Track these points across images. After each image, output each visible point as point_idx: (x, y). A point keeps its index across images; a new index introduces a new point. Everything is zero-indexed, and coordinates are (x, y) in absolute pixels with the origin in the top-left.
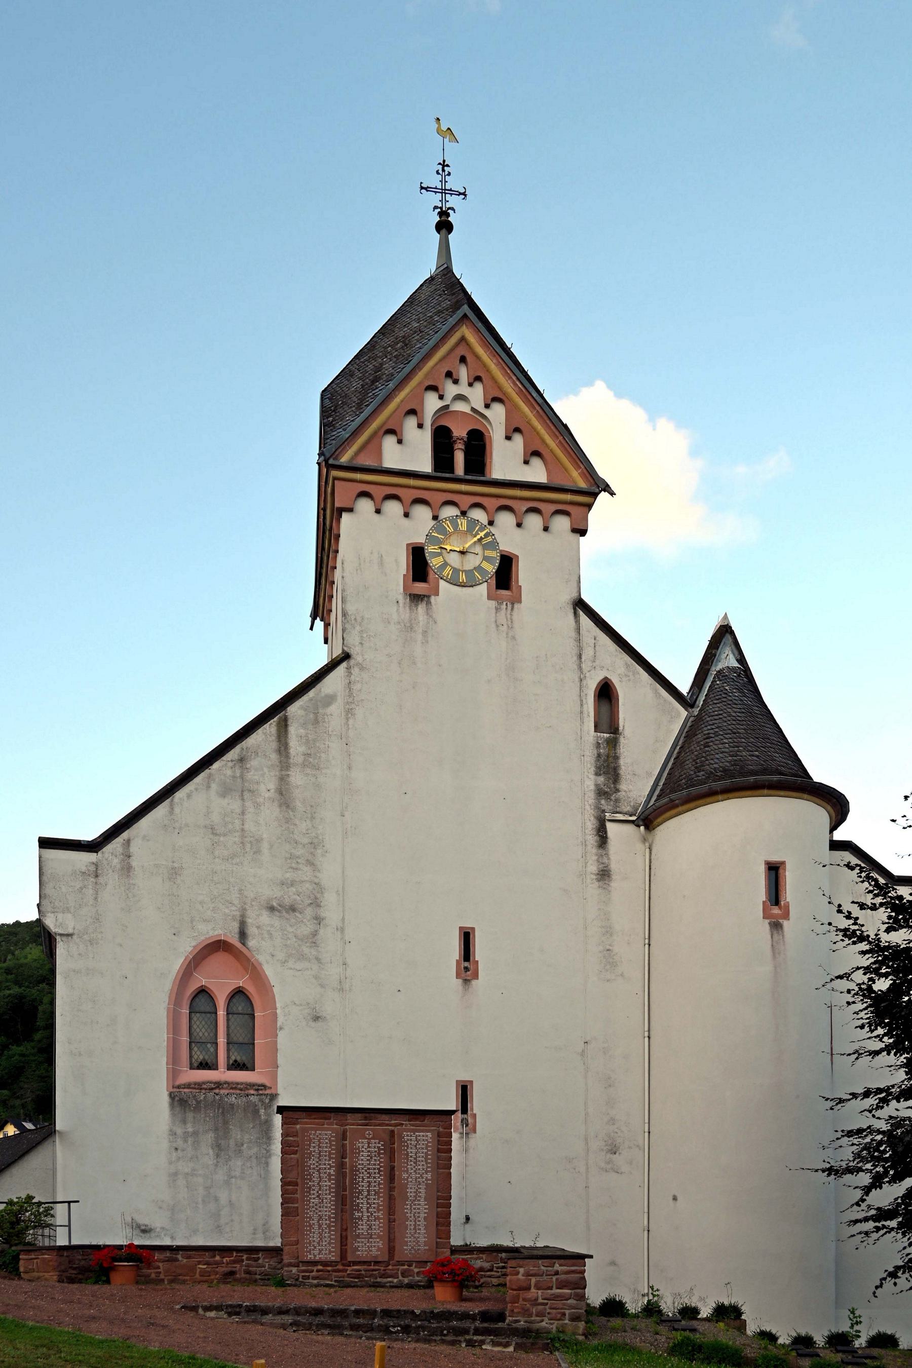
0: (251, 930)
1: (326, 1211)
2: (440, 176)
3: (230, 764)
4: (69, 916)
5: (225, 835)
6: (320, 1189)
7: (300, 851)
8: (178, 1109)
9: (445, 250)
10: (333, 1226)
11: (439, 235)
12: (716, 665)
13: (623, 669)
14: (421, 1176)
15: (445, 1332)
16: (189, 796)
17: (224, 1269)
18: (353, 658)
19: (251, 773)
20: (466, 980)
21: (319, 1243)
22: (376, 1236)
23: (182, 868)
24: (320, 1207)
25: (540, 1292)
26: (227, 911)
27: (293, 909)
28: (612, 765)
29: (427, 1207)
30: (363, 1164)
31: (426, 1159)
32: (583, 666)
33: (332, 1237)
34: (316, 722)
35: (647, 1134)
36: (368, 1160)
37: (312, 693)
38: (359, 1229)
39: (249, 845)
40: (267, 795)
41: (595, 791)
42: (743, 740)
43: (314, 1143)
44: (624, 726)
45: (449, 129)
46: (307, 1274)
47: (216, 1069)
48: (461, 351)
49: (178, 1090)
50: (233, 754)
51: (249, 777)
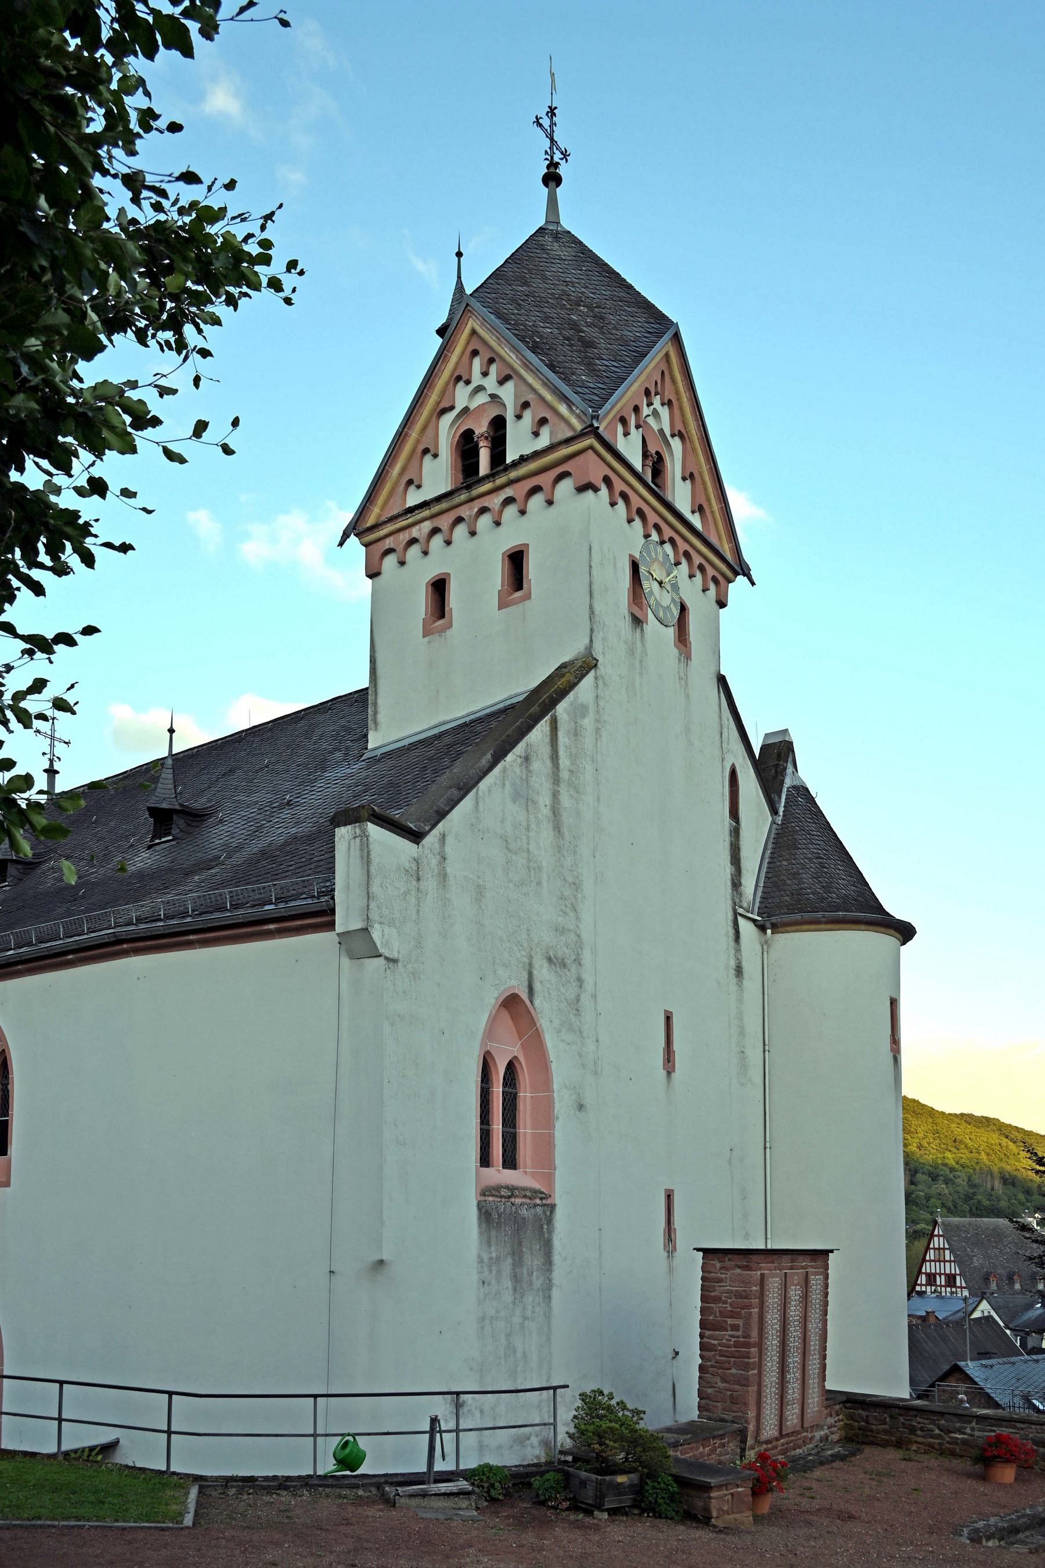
9: (552, 203)
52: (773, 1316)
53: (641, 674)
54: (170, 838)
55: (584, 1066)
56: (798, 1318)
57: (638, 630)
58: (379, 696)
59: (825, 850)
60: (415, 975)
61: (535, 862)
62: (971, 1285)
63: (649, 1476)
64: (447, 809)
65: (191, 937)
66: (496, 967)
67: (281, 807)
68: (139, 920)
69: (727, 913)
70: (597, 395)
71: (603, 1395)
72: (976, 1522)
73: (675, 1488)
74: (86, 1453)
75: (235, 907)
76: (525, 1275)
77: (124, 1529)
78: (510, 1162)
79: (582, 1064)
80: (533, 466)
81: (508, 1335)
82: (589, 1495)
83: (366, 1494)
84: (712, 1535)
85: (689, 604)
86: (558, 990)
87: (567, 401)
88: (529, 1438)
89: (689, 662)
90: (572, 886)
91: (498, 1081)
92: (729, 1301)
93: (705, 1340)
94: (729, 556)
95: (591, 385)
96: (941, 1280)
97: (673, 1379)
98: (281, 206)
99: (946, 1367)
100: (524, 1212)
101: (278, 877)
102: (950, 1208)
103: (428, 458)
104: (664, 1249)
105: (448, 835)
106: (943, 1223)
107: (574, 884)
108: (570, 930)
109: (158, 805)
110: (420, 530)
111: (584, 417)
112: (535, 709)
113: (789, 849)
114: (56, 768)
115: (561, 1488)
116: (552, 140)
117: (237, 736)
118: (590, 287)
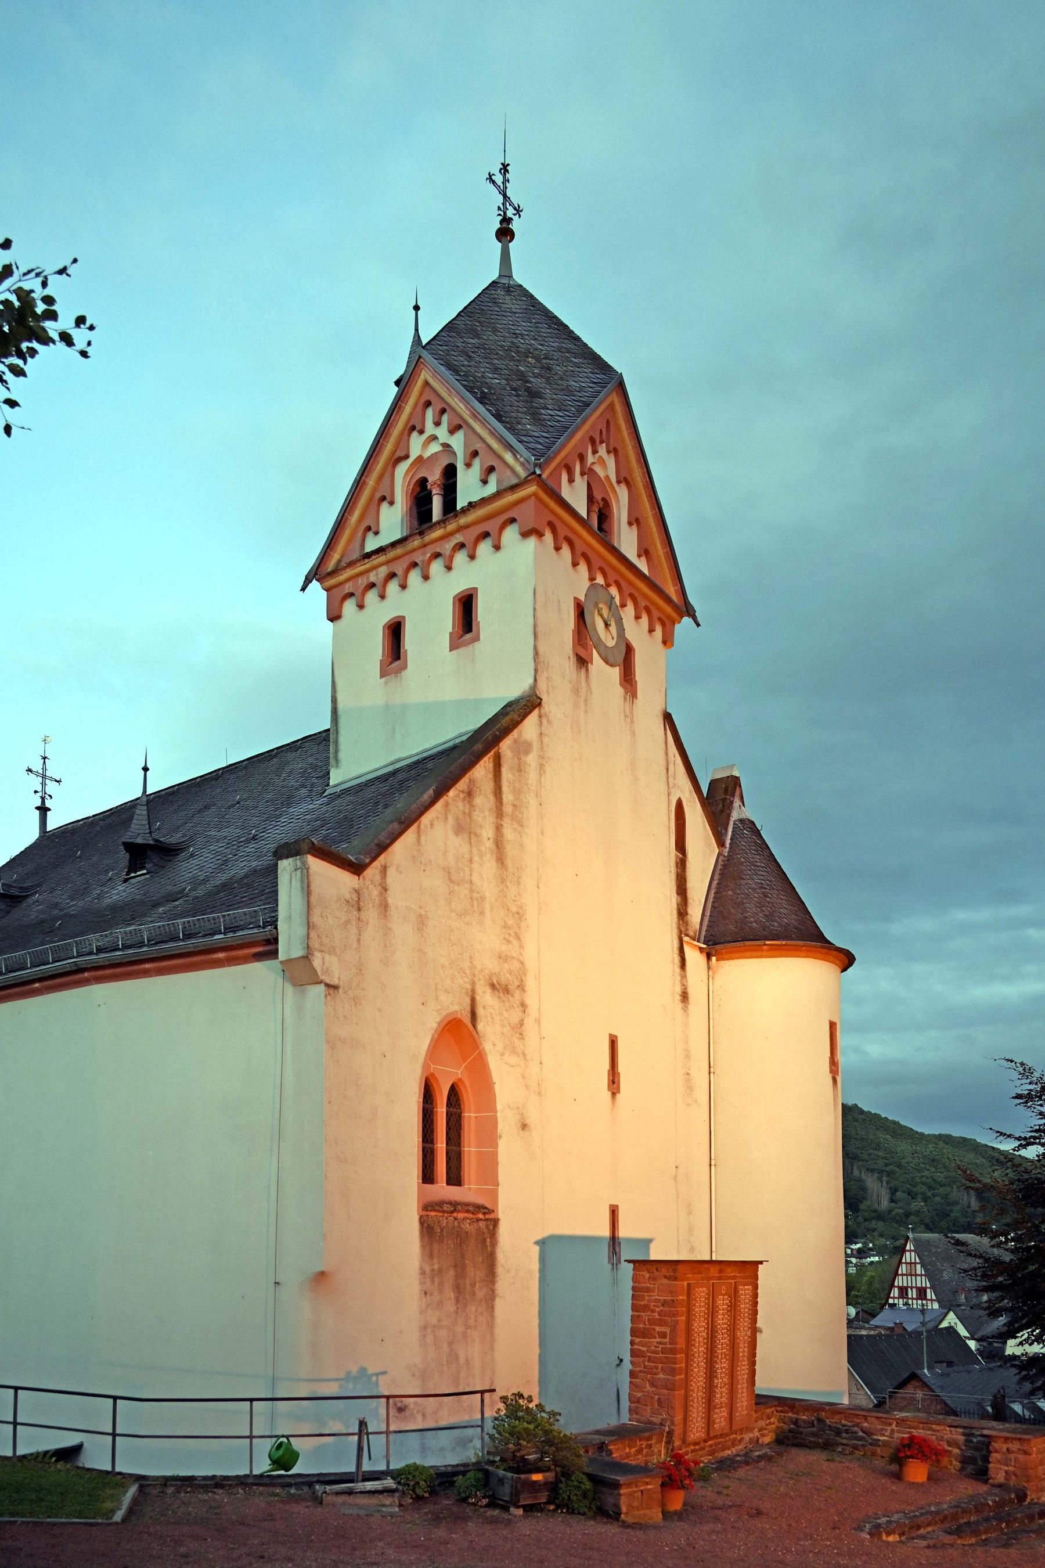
52: (700, 1324)
53: (586, 711)
54: (145, 871)
55: (527, 1087)
56: (726, 1326)
57: (583, 670)
58: (340, 735)
59: (769, 881)
60: (356, 1001)
61: (478, 893)
62: (940, 1297)
63: (563, 1474)
64: (388, 842)
65: (147, 966)
66: (438, 993)
67: (247, 842)
68: (100, 950)
69: (672, 941)
70: (540, 444)
71: (523, 1398)
72: (879, 1518)
73: (588, 1485)
74: (41, 1456)
75: (188, 936)
76: (468, 1287)
77: (54, 1524)
78: (455, 1178)
79: (526, 1085)
80: (480, 512)
81: (450, 1344)
82: (505, 1493)
83: (299, 1492)
84: (618, 1530)
85: (634, 644)
86: (501, 1014)
87: (512, 449)
88: (472, 1441)
89: (635, 699)
90: (516, 915)
91: (442, 1103)
92: (657, 1309)
93: (636, 1347)
94: (674, 598)
95: (536, 434)
96: (912, 1293)
97: (617, 1384)
98: (75, 261)
99: (906, 1375)
100: (466, 1226)
101: (232, 907)
102: (928, 1225)
103: (384, 506)
104: (609, 1262)
105: (389, 867)
106: (915, 1239)
107: (518, 913)
108: (513, 958)
109: (132, 840)
110: (377, 575)
111: (527, 465)
112: (478, 747)
113: (734, 879)
114: (47, 805)
115: (481, 1485)
116: (505, 196)
117: (215, 774)
118: (539, 339)
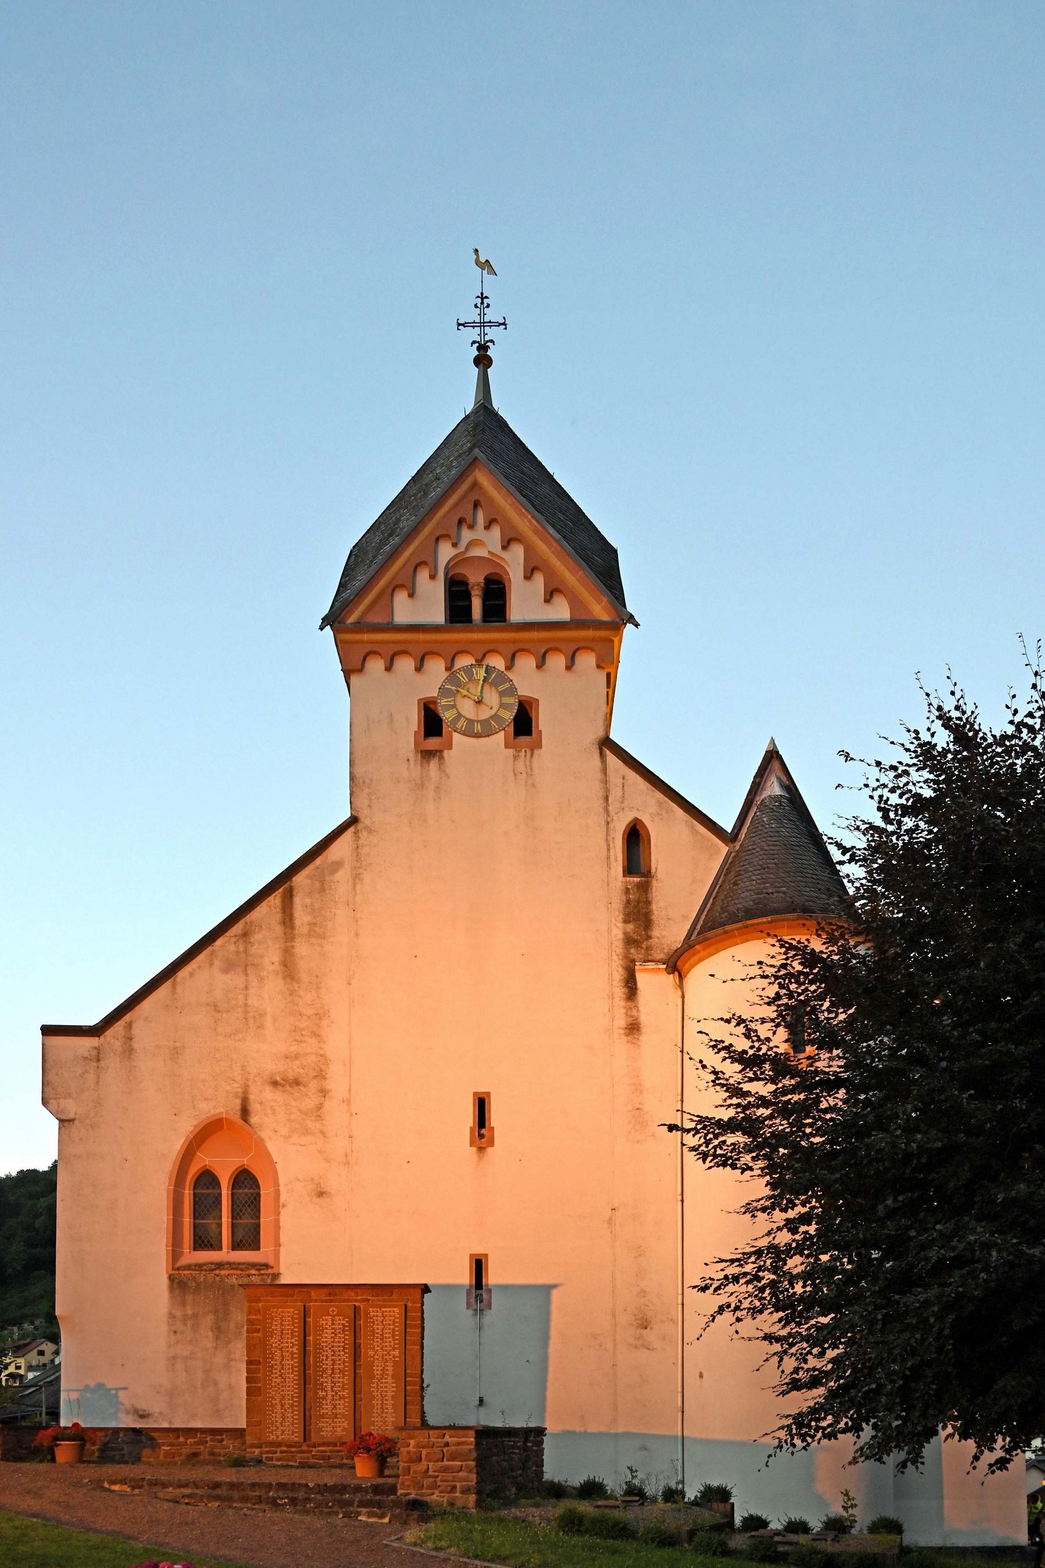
0: (254, 1106)
1: (289, 1391)
2: (479, 309)
3: (233, 940)
4: (71, 1101)
5: (228, 1011)
6: (282, 1368)
7: (304, 1024)
8: (177, 1292)
10: (296, 1406)
11: (477, 369)
12: (760, 795)
13: (655, 807)
14: (388, 1353)
15: (330, 1504)
16: (191, 974)
17: (188, 1450)
18: (362, 822)
19: (255, 947)
20: (480, 1148)
21: (281, 1423)
22: (341, 1416)
23: (184, 1047)
24: (282, 1387)
25: (431, 1464)
26: (229, 1088)
27: (297, 1082)
28: (644, 911)
29: (394, 1385)
30: (326, 1342)
31: (394, 1335)
32: (610, 808)
33: (295, 1417)
34: (322, 890)
35: (680, 1307)
36: (332, 1337)
37: (318, 861)
38: (323, 1409)
39: (251, 1021)
40: (271, 968)
41: (623, 939)
42: (772, 876)
43: (276, 1321)
44: (656, 869)
45: (487, 261)
46: (270, 1455)
47: (221, 1249)
48: (474, 496)
49: (177, 1272)
50: (237, 929)
51: (254, 951)
